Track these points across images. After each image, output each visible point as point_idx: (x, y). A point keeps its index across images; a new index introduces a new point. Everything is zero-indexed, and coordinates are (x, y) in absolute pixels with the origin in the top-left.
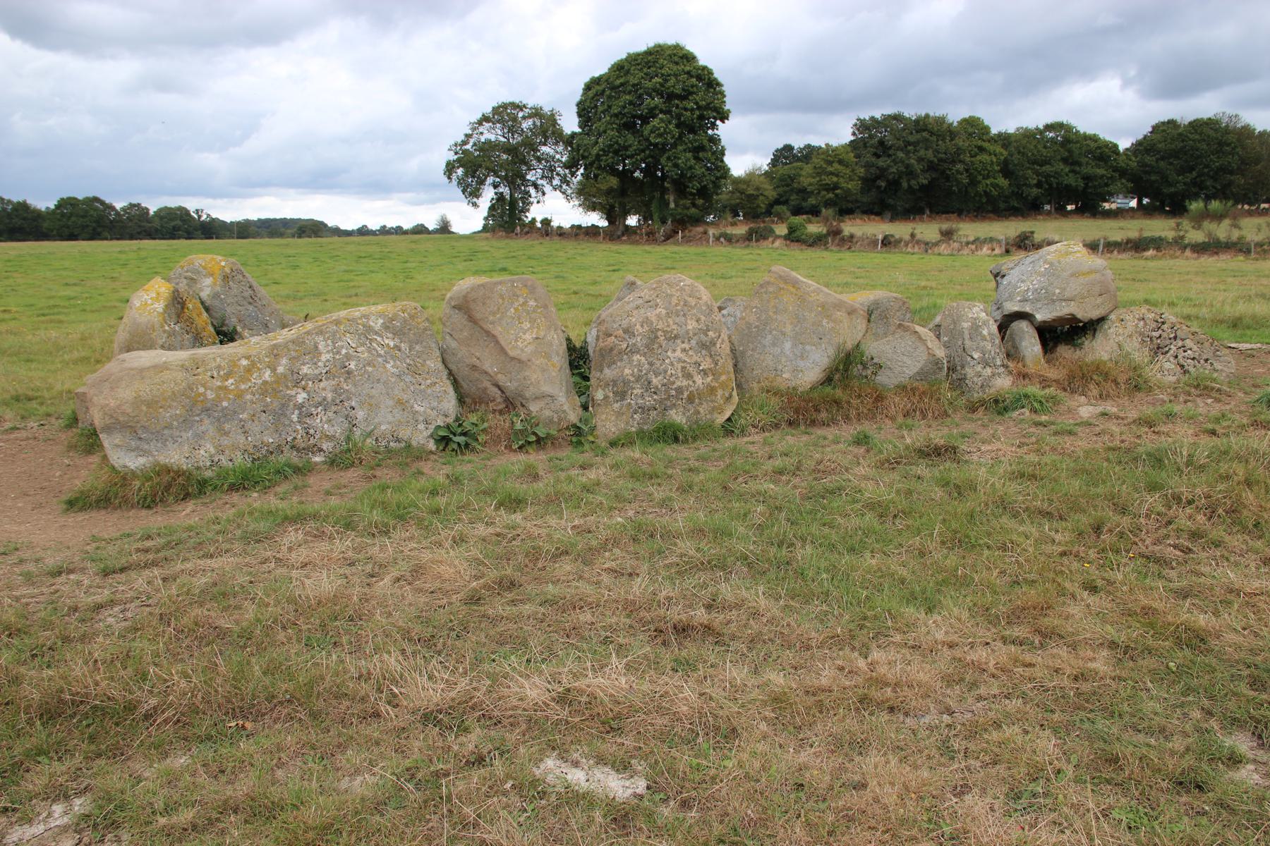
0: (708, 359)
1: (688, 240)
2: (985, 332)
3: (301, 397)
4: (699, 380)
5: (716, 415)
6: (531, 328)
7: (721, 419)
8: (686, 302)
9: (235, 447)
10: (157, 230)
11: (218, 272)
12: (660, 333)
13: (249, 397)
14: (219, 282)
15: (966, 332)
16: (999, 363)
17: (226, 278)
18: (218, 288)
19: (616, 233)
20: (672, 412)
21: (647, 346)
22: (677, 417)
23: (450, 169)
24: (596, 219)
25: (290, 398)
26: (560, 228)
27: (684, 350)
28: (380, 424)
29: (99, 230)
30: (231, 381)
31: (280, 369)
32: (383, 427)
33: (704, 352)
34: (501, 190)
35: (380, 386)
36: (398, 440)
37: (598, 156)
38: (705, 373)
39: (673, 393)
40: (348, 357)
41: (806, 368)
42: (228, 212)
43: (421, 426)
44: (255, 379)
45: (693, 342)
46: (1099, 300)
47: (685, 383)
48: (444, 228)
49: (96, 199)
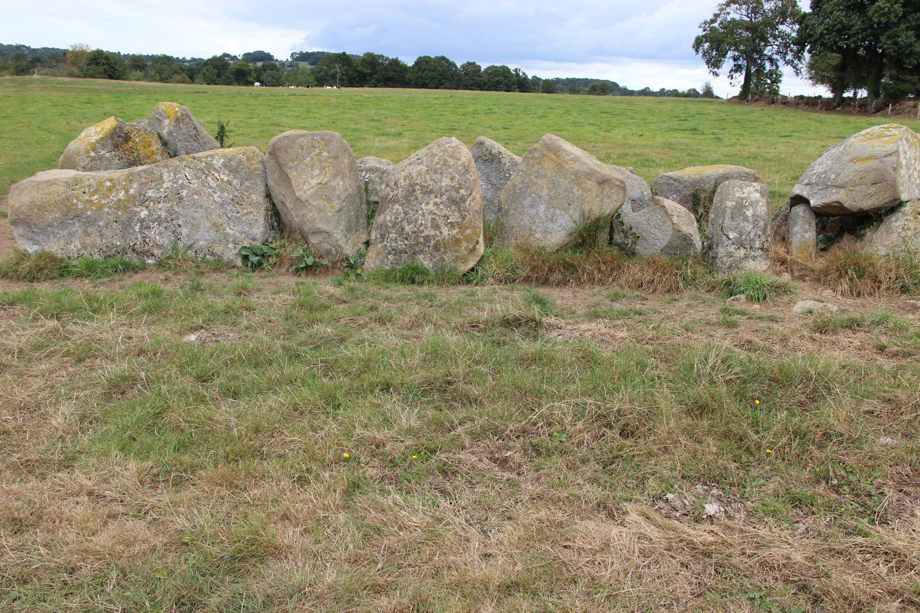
0: (456, 214)
1: (897, 113)
2: (749, 213)
3: (144, 213)
4: (445, 231)
5: (459, 264)
6: (319, 175)
7: (464, 268)
8: (446, 161)
9: (93, 246)
10: (485, 83)
11: (172, 115)
12: (417, 187)
13: (106, 210)
14: (173, 123)
15: (729, 211)
16: (757, 245)
17: (178, 120)
18: (172, 128)
19: (836, 105)
20: (421, 257)
21: (405, 198)
22: (425, 262)
23: (698, 43)
24: (824, 91)
25: (136, 213)
26: (784, 97)
27: (436, 204)
28: (199, 240)
29: (443, 81)
30: (96, 197)
31: (132, 191)
32: (201, 243)
33: (453, 207)
34: (740, 63)
35: (202, 211)
36: (213, 254)
37: (822, 34)
38: (452, 225)
39: (422, 240)
40: (183, 186)
41: (552, 228)
42: (546, 73)
43: (231, 246)
44: (113, 197)
45: (445, 197)
46: (872, 190)
47: (432, 233)
48: (708, 93)
49: (443, 58)
